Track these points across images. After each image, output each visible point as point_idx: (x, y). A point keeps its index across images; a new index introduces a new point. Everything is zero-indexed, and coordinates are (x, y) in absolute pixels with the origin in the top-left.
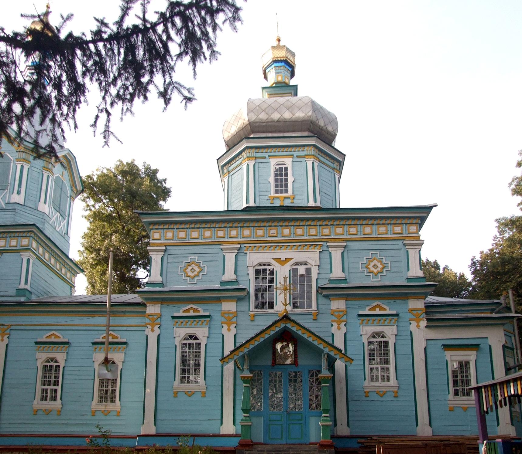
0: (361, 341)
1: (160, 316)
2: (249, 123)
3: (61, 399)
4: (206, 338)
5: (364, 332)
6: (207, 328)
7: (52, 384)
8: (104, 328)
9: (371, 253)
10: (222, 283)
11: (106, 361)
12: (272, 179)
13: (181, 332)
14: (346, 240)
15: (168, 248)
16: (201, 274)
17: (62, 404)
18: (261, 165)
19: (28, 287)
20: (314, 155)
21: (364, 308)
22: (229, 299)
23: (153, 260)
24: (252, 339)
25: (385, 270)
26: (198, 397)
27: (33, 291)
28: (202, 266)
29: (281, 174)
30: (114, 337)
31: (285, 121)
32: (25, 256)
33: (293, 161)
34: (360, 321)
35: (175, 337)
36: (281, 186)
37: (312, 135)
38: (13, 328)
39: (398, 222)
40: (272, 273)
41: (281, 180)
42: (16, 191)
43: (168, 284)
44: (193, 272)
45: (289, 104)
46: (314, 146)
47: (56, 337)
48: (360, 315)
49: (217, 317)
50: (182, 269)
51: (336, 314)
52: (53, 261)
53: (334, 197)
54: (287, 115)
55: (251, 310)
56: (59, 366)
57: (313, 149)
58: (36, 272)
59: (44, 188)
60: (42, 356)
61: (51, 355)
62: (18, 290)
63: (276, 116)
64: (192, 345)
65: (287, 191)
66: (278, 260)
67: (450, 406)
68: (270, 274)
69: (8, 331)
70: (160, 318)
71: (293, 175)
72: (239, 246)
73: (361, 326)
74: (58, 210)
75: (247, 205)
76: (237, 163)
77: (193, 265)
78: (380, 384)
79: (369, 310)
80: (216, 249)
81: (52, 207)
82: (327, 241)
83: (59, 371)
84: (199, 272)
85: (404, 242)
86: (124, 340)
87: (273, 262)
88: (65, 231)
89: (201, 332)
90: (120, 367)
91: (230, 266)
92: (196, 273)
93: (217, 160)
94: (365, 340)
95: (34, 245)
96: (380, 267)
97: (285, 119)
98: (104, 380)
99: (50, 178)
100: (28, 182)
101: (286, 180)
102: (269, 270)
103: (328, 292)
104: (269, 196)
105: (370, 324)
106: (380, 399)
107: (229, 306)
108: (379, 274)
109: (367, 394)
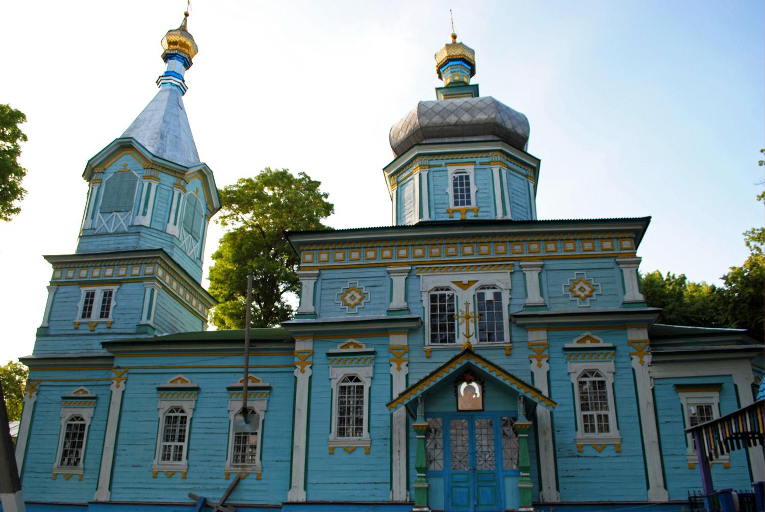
0: (569, 380)
1: (312, 353)
2: (421, 128)
3: (187, 458)
4: (370, 379)
5: (573, 370)
6: (372, 367)
8: (242, 370)
11: (245, 411)
12: (450, 190)
13: (339, 372)
15: (323, 272)
16: (363, 302)
17: (188, 465)
18: (436, 174)
19: (151, 322)
20: (500, 162)
21: (570, 339)
22: (398, 331)
24: (426, 378)
25: (594, 294)
26: (360, 453)
27: (156, 327)
29: (462, 183)
30: (255, 380)
31: (464, 125)
33: (475, 169)
34: (566, 356)
35: (330, 379)
36: (462, 197)
41: (462, 191)
45: (468, 106)
46: (501, 151)
47: (183, 381)
48: (565, 349)
49: (383, 352)
51: (535, 347)
52: (181, 291)
54: (466, 118)
55: (426, 344)
56: (186, 417)
59: (174, 207)
60: (68, 413)
62: (140, 326)
63: (453, 119)
64: (352, 389)
65: (469, 203)
66: (459, 284)
67: (689, 462)
69: (125, 376)
70: (408, 352)
71: (476, 184)
72: (410, 268)
73: (569, 363)
74: (190, 231)
75: (421, 220)
77: (353, 292)
78: (597, 435)
81: (182, 228)
82: (519, 260)
83: (185, 423)
84: (360, 300)
85: (617, 260)
86: (267, 385)
87: (453, 286)
88: (198, 256)
89: (364, 372)
90: (261, 418)
91: (400, 292)
92: (356, 301)
93: (384, 169)
94: (574, 379)
95: (160, 272)
96: (588, 289)
98: (241, 433)
99: (182, 196)
100: (156, 202)
101: (468, 190)
102: (448, 295)
103: (524, 320)
104: (447, 207)
108: (588, 299)
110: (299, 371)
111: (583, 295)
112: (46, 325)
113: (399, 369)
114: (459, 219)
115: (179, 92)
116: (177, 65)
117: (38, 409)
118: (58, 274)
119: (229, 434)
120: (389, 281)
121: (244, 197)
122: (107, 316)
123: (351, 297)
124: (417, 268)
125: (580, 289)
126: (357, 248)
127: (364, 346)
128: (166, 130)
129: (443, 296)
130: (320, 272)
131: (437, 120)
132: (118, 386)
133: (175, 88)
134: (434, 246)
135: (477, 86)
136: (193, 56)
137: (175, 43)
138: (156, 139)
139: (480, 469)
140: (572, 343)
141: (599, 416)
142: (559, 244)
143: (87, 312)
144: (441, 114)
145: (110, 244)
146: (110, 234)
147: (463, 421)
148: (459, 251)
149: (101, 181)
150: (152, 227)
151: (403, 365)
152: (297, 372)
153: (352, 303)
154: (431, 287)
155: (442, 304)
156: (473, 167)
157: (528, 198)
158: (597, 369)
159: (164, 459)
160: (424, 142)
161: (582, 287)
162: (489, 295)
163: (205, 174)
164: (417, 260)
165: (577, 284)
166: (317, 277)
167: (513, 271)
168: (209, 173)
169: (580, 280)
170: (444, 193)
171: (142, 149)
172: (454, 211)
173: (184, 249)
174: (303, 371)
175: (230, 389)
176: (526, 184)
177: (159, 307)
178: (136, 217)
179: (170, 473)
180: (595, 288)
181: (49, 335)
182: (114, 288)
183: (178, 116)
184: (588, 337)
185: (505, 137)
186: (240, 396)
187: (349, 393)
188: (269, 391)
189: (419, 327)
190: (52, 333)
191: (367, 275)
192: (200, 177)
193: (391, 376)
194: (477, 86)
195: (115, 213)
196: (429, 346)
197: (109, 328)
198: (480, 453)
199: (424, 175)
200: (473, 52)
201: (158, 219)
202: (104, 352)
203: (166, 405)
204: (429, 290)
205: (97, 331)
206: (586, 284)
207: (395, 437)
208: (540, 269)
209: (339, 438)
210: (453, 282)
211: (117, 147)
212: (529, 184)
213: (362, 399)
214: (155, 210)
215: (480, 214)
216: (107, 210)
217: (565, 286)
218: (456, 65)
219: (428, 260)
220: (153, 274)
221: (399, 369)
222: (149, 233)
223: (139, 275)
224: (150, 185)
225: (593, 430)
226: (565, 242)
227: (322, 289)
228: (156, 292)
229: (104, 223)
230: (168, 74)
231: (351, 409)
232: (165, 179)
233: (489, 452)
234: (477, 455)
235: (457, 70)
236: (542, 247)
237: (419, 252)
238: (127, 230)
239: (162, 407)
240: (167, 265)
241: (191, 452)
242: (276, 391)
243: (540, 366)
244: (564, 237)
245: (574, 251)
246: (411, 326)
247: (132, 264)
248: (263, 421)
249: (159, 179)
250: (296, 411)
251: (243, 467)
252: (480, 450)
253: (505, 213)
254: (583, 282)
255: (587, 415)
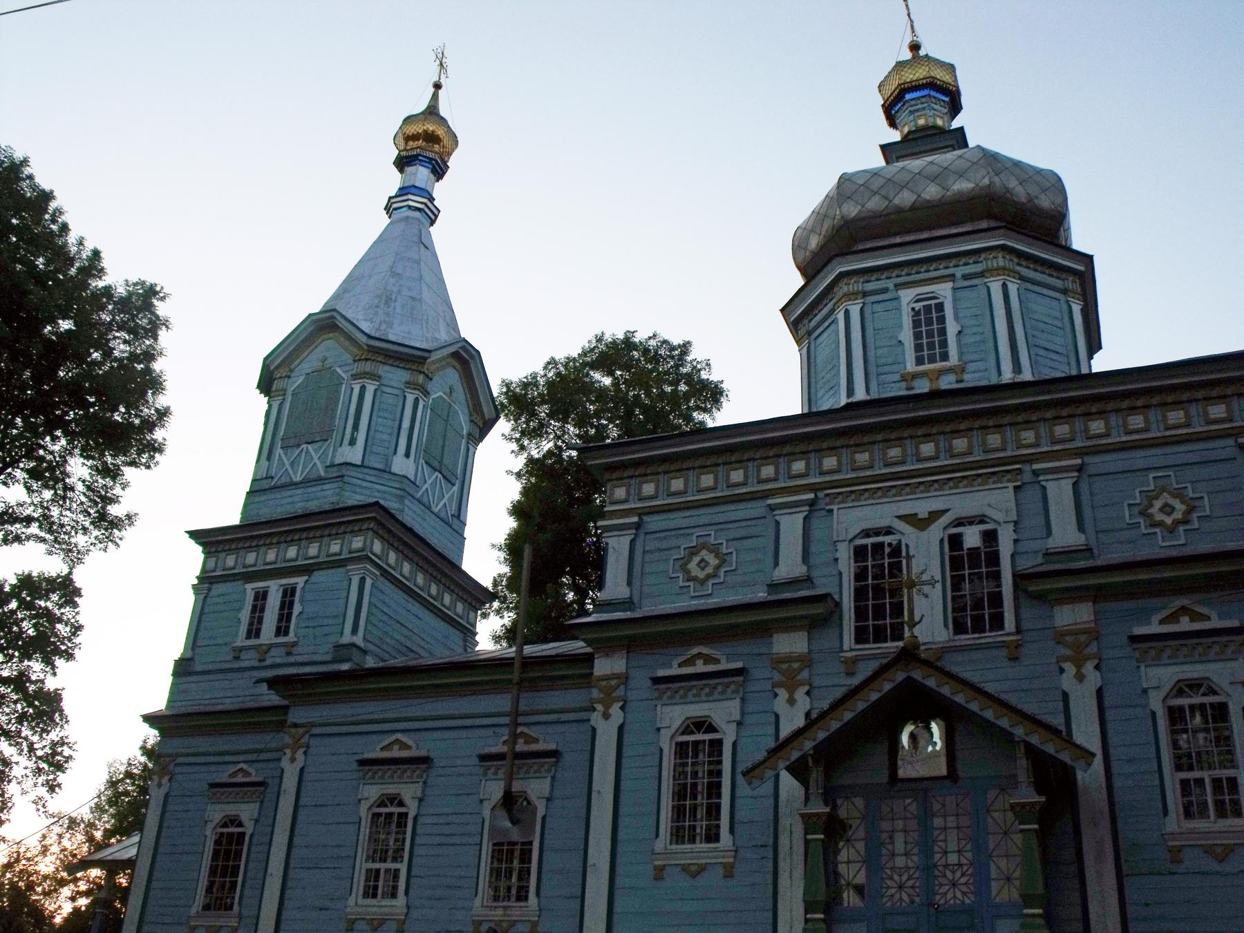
0: (1145, 706)
1: (624, 679)
3: (407, 893)
5: (1154, 683)
7: (389, 860)
8: (506, 720)
9: (1151, 476)
10: (773, 587)
11: (509, 801)
12: (907, 336)
13: (674, 715)
14: (1079, 453)
15: (646, 518)
17: (408, 907)
18: (877, 307)
19: (358, 640)
20: (1004, 268)
22: (788, 626)
23: (610, 550)
25: (1195, 515)
26: (713, 878)
27: (371, 647)
28: (725, 551)
29: (929, 320)
30: (530, 740)
31: (931, 205)
32: (355, 573)
33: (954, 289)
34: (1137, 654)
35: (659, 730)
37: (993, 224)
38: (315, 731)
39: (1215, 393)
40: (896, 551)
41: (930, 334)
42: (346, 442)
43: (643, 602)
44: (703, 569)
45: (935, 169)
46: (1003, 248)
47: (404, 746)
48: (1134, 639)
50: (679, 563)
52: (420, 579)
53: (1072, 355)
54: (932, 192)
55: (846, 647)
56: (406, 814)
57: (1000, 255)
58: (380, 605)
59: (406, 424)
60: (216, 813)
61: (391, 789)
62: (338, 647)
63: (905, 199)
64: (701, 747)
65: (945, 357)
66: (911, 519)
68: (890, 555)
69: (305, 739)
70: (625, 684)
71: (956, 318)
72: (811, 496)
73: (1143, 668)
74: (436, 464)
76: (825, 311)
77: (704, 553)
78: (1211, 824)
79: (1162, 622)
80: (757, 508)
81: (422, 461)
82: (1030, 459)
83: (406, 826)
84: (718, 568)
86: (552, 746)
89: (723, 712)
90: (541, 812)
91: (793, 547)
92: (709, 570)
93: (782, 310)
94: (1156, 703)
95: (377, 546)
96: (1180, 507)
97: (929, 201)
98: (503, 844)
100: (374, 418)
101: (943, 332)
102: (890, 545)
103: (1048, 582)
105: (1165, 660)
106: (1216, 867)
107: (791, 643)
108: (1181, 529)
109: (1176, 855)
110: (600, 717)
111: (1169, 521)
112: (189, 655)
113: (791, 701)
114: (926, 390)
115: (423, 220)
116: (421, 174)
117: (170, 807)
118: (211, 564)
119: (481, 844)
120: (772, 525)
121: (558, 396)
122: (286, 633)
123: (698, 564)
124: (827, 495)
125: (1161, 510)
126: (712, 466)
127: (723, 660)
128: (395, 289)
129: (879, 547)
130: (641, 519)
131: (875, 204)
132: (293, 760)
133: (417, 214)
134: (860, 449)
135: (962, 129)
136: (450, 154)
137: (415, 137)
138: (377, 307)
139: (942, 902)
140: (1149, 624)
141: (1216, 782)
142: (1114, 420)
143: (254, 631)
144: (883, 192)
145: (294, 502)
146: (296, 484)
147: (908, 801)
148: (909, 452)
149: (284, 392)
150: (367, 463)
151: (1089, 667)
152: (596, 719)
153: (701, 575)
154: (855, 530)
155: (881, 569)
156: (950, 284)
157: (1070, 336)
158: (1208, 678)
159: (366, 895)
160: (846, 249)
161: (1166, 505)
162: (972, 538)
163: (466, 360)
164: (828, 478)
165: (1157, 498)
166: (637, 529)
167: (1018, 483)
168: (472, 357)
169: (1163, 489)
170: (894, 342)
171: (350, 327)
172: (915, 376)
173: (425, 500)
174: (606, 716)
175: (484, 758)
176: (1065, 306)
177: (374, 611)
178: (340, 450)
179: (375, 923)
180: (1197, 504)
181: (190, 674)
182: (300, 581)
183: (418, 262)
184: (1184, 610)
185: (1024, 223)
186: (503, 770)
187: (696, 755)
188: (554, 760)
189: (832, 613)
190: (199, 668)
191: (732, 516)
192: (458, 366)
193: (777, 716)
194: (962, 129)
195: (304, 446)
196: (852, 650)
197: (289, 654)
198: (941, 868)
199: (855, 310)
200: (951, 68)
201: (375, 449)
202: (273, 699)
203: (372, 792)
204: (850, 537)
205: (268, 662)
206: (1175, 496)
207: (784, 840)
208: (1076, 474)
209: (674, 847)
210: (898, 517)
211: (310, 329)
212: (1070, 307)
213: (718, 767)
214: (371, 433)
215: (966, 377)
216: (292, 442)
217: (1130, 505)
218: (918, 98)
219: (849, 476)
220: (363, 550)
221: (791, 701)
222: (360, 476)
223: (340, 554)
224: (363, 388)
225: (1203, 813)
226: (1125, 413)
227: (644, 552)
228: (369, 582)
229: (288, 466)
230: (403, 191)
231: (700, 788)
232: (390, 376)
233: (960, 865)
234: (936, 873)
235: (920, 106)
236: (1077, 428)
237: (830, 462)
238: (323, 474)
239: (366, 795)
240: (390, 531)
241: (413, 880)
242: (567, 758)
243: (1080, 677)
244: (1125, 404)
245: (1147, 430)
246: (815, 612)
247: (352, 532)
248: (544, 818)
249: (380, 377)
250: (594, 795)
251: (505, 908)
252: (943, 861)
253: (1017, 368)
254: (1170, 493)
255: (1188, 780)
